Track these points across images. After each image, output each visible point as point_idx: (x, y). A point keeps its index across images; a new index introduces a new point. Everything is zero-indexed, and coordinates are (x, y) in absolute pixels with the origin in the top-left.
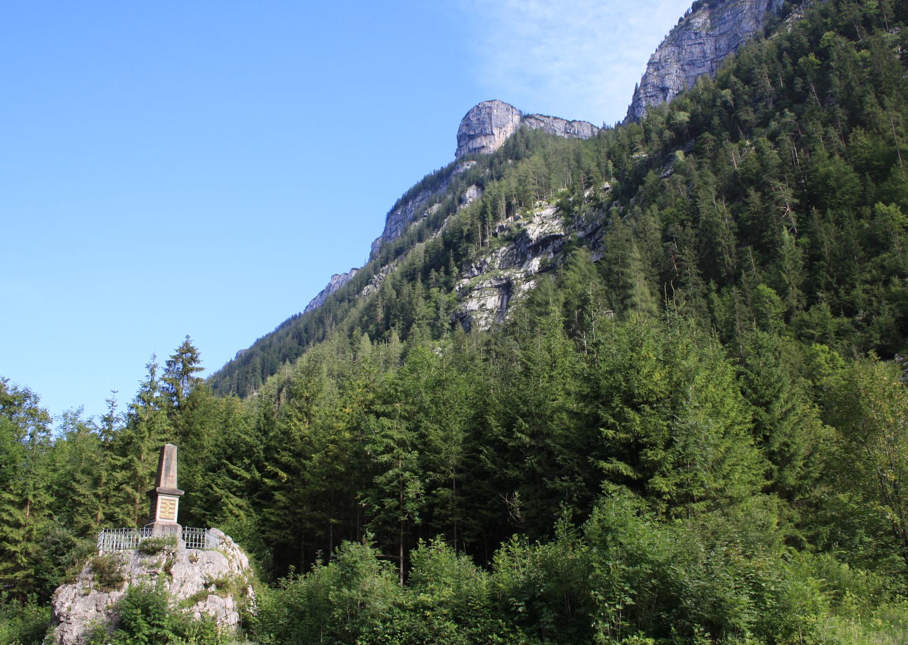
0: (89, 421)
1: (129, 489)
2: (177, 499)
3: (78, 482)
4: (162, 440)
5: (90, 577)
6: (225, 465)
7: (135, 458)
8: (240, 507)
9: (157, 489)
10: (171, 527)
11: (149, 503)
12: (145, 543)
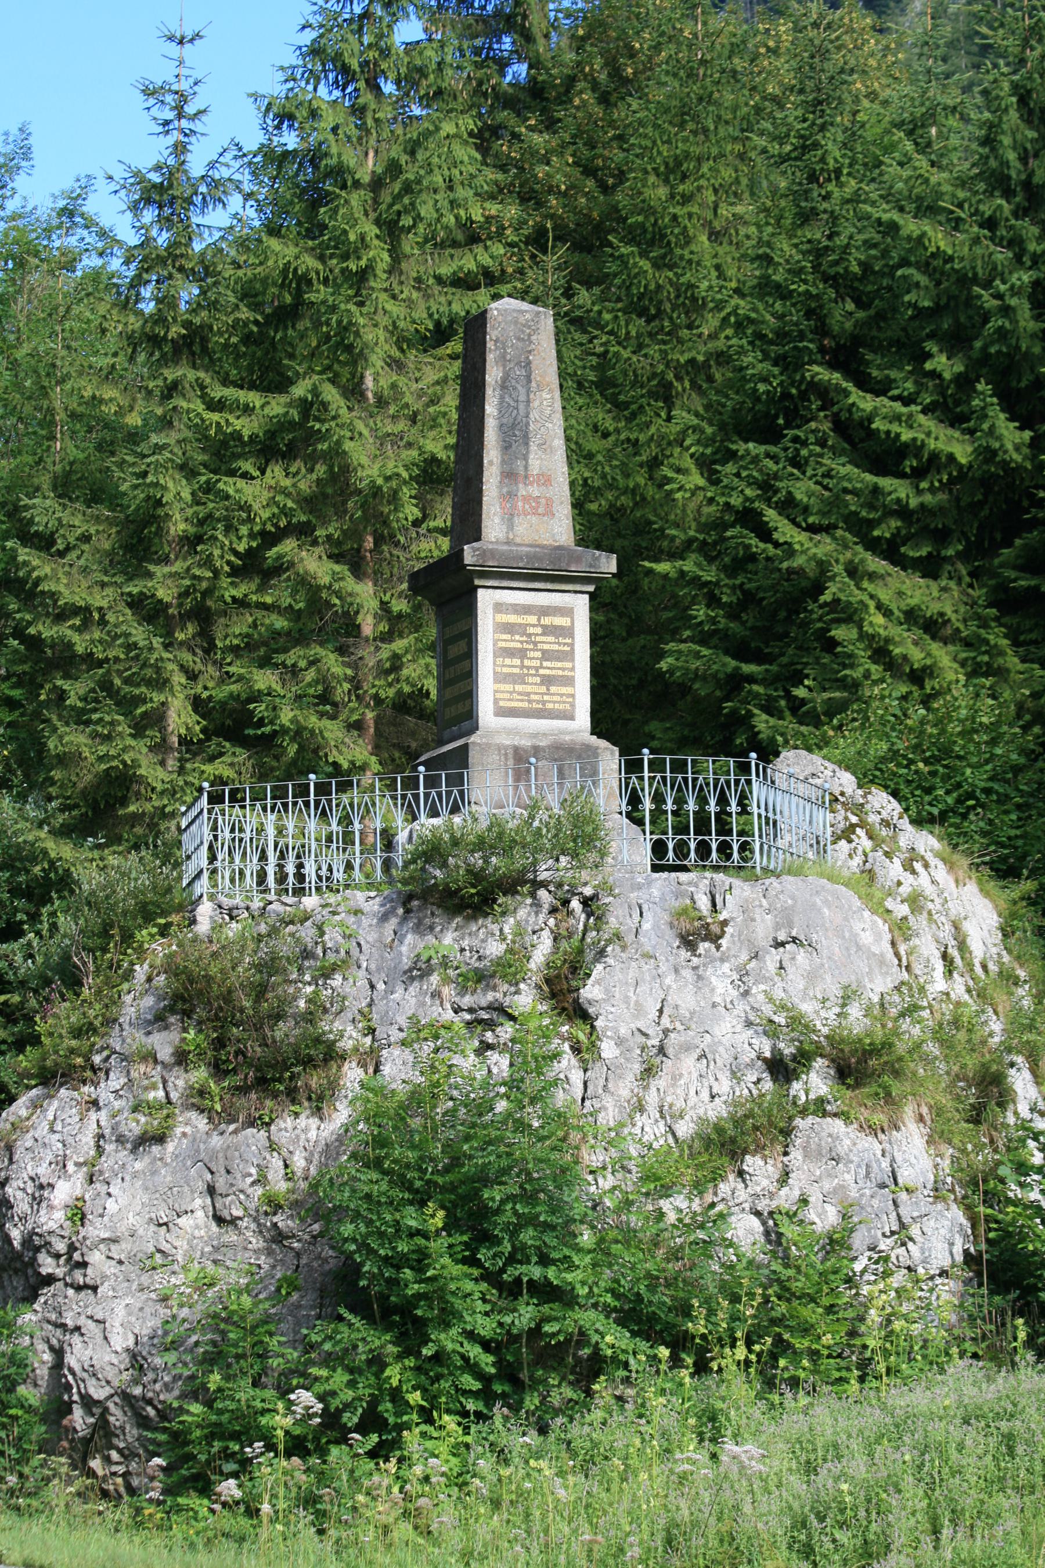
0: (68, 212)
1: (316, 565)
2: (580, 605)
3: (44, 542)
4: (465, 283)
5: (164, 1044)
6: (826, 395)
7: (331, 394)
8: (932, 627)
9: (470, 555)
10: (562, 754)
11: (432, 632)
12: (432, 852)
